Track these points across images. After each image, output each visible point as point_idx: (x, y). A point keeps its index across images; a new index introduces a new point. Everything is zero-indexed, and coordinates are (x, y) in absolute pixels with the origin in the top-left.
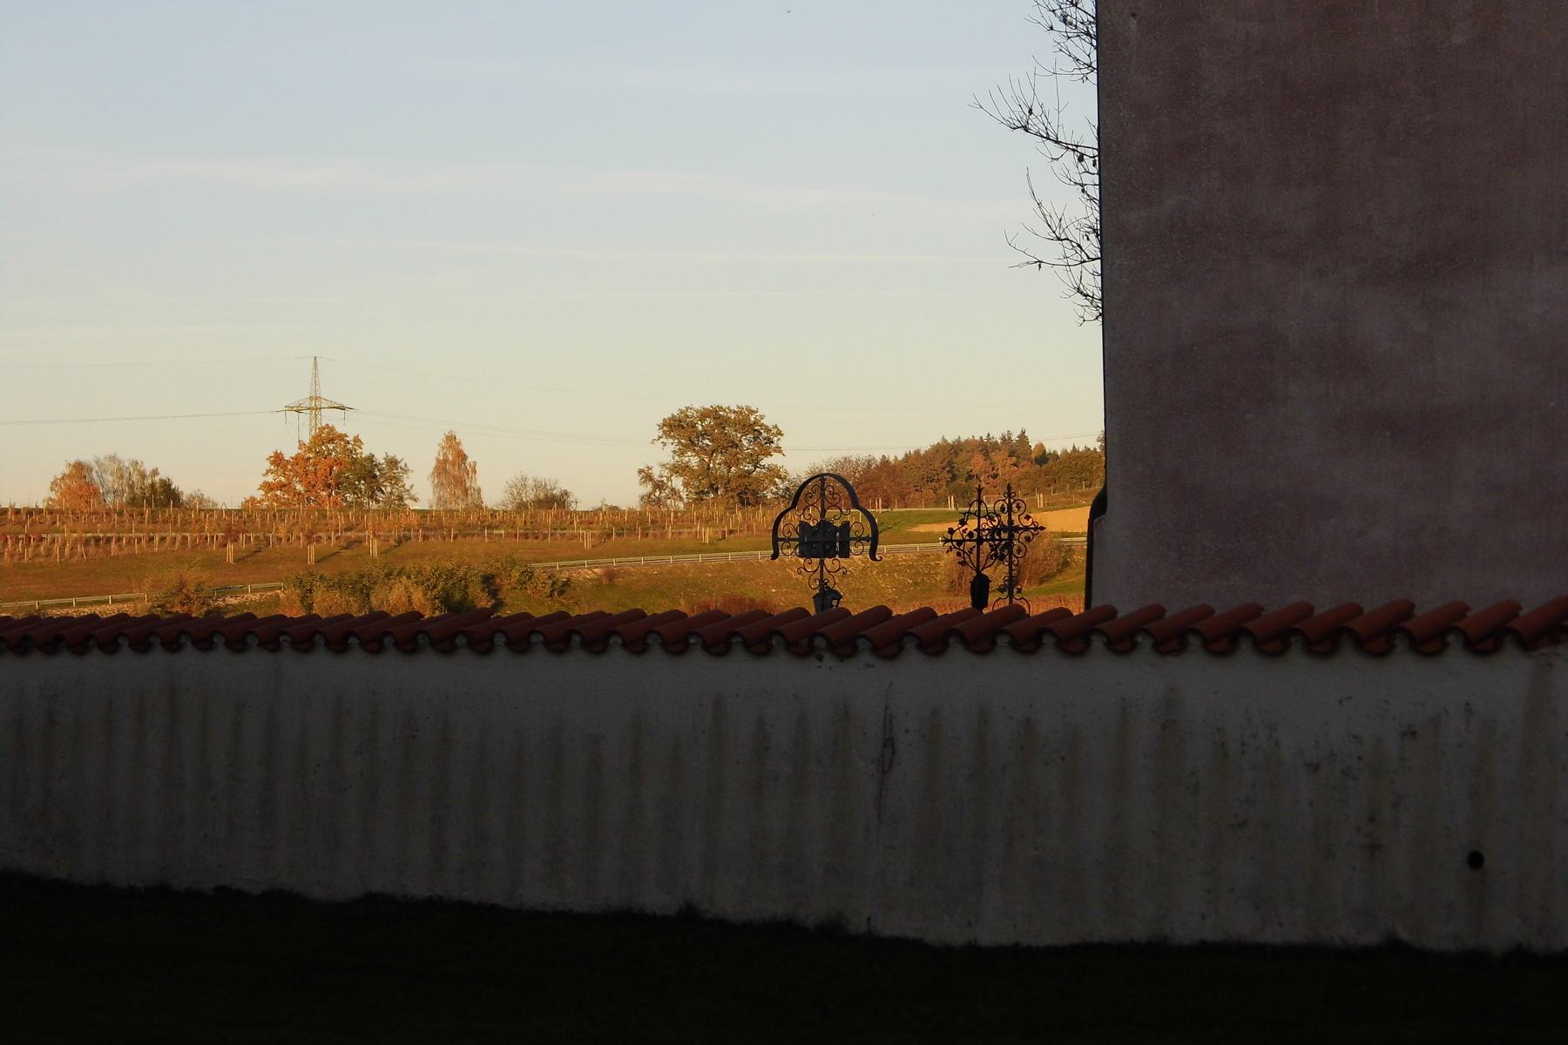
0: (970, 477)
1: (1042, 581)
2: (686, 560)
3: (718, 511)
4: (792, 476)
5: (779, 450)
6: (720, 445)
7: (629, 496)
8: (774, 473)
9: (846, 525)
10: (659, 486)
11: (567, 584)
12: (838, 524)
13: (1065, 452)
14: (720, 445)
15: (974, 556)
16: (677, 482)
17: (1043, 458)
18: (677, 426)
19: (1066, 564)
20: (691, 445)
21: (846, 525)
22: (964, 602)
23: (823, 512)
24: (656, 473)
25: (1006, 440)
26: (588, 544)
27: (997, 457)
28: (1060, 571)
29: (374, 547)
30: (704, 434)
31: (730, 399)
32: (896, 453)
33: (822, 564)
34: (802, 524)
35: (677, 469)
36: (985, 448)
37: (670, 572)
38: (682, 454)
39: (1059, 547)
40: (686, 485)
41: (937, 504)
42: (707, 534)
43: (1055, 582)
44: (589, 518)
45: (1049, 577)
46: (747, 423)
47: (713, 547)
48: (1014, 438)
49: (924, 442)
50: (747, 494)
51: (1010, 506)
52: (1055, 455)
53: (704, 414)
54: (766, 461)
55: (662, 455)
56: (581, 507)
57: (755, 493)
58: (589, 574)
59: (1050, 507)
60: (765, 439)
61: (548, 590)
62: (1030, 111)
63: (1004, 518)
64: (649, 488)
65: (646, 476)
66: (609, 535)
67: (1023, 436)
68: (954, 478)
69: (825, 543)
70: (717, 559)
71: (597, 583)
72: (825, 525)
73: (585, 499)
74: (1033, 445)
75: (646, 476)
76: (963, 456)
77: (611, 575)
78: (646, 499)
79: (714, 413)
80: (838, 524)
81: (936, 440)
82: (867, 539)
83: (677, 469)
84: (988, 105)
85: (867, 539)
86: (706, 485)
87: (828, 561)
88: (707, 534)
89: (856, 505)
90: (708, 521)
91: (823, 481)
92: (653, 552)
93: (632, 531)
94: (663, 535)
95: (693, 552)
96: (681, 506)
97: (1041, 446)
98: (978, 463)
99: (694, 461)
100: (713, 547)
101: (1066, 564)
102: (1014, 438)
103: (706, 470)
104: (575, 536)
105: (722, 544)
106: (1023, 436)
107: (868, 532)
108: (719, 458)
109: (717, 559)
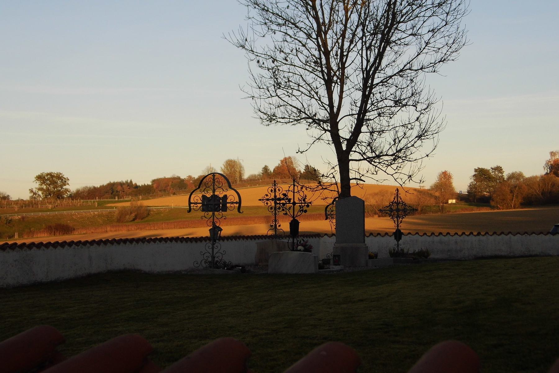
0: (117, 192)
1: (142, 219)
2: (44, 214)
3: (53, 200)
4: (72, 191)
5: (68, 184)
6: (52, 183)
7: (26, 196)
8: (67, 190)
9: (225, 197)
10: (35, 194)
11: (11, 220)
12: (221, 196)
14: (52, 183)
15: (291, 211)
16: (40, 193)
17: (136, 187)
18: (40, 178)
19: (148, 214)
20: (44, 183)
21: (225, 197)
22: (334, 237)
24: (34, 190)
25: (127, 182)
26: (16, 210)
27: (124, 186)
30: (48, 180)
31: (55, 170)
32: (98, 185)
33: (214, 214)
35: (40, 189)
36: (121, 184)
37: (40, 217)
38: (41, 185)
39: (147, 210)
40: (42, 193)
41: (112, 198)
42: (50, 206)
43: (146, 219)
44: (17, 202)
46: (59, 177)
47: (52, 210)
48: (129, 181)
49: (105, 183)
50: (59, 195)
51: (275, 190)
52: (139, 186)
53: (48, 174)
54: (64, 187)
55: (36, 185)
56: (13, 199)
57: (61, 196)
58: (17, 218)
59: (143, 199)
60: (64, 181)
61: (5, 222)
62: (246, 40)
63: (273, 194)
64: (32, 194)
65: (31, 191)
66: (22, 207)
67: (131, 181)
68: (113, 192)
69: (215, 205)
70: (52, 213)
71: (19, 220)
72: (214, 197)
73: (14, 197)
74: (134, 183)
75: (31, 191)
76: (115, 186)
77: (23, 218)
78: (32, 197)
79: (50, 174)
80: (221, 196)
81: (108, 182)
82: (236, 203)
83: (40, 189)
84: (228, 37)
85: (236, 203)
86: (47, 193)
87: (216, 213)
88: (50, 206)
90: (50, 203)
92: (35, 211)
93: (29, 206)
94: (38, 207)
95: (46, 211)
96: (41, 199)
97: (136, 184)
98: (119, 188)
99: (45, 187)
100: (52, 210)
101: (148, 214)
102: (129, 181)
103: (48, 189)
104: (13, 207)
105: (54, 209)
106: (131, 181)
107: (237, 200)
108: (52, 186)
109: (52, 213)
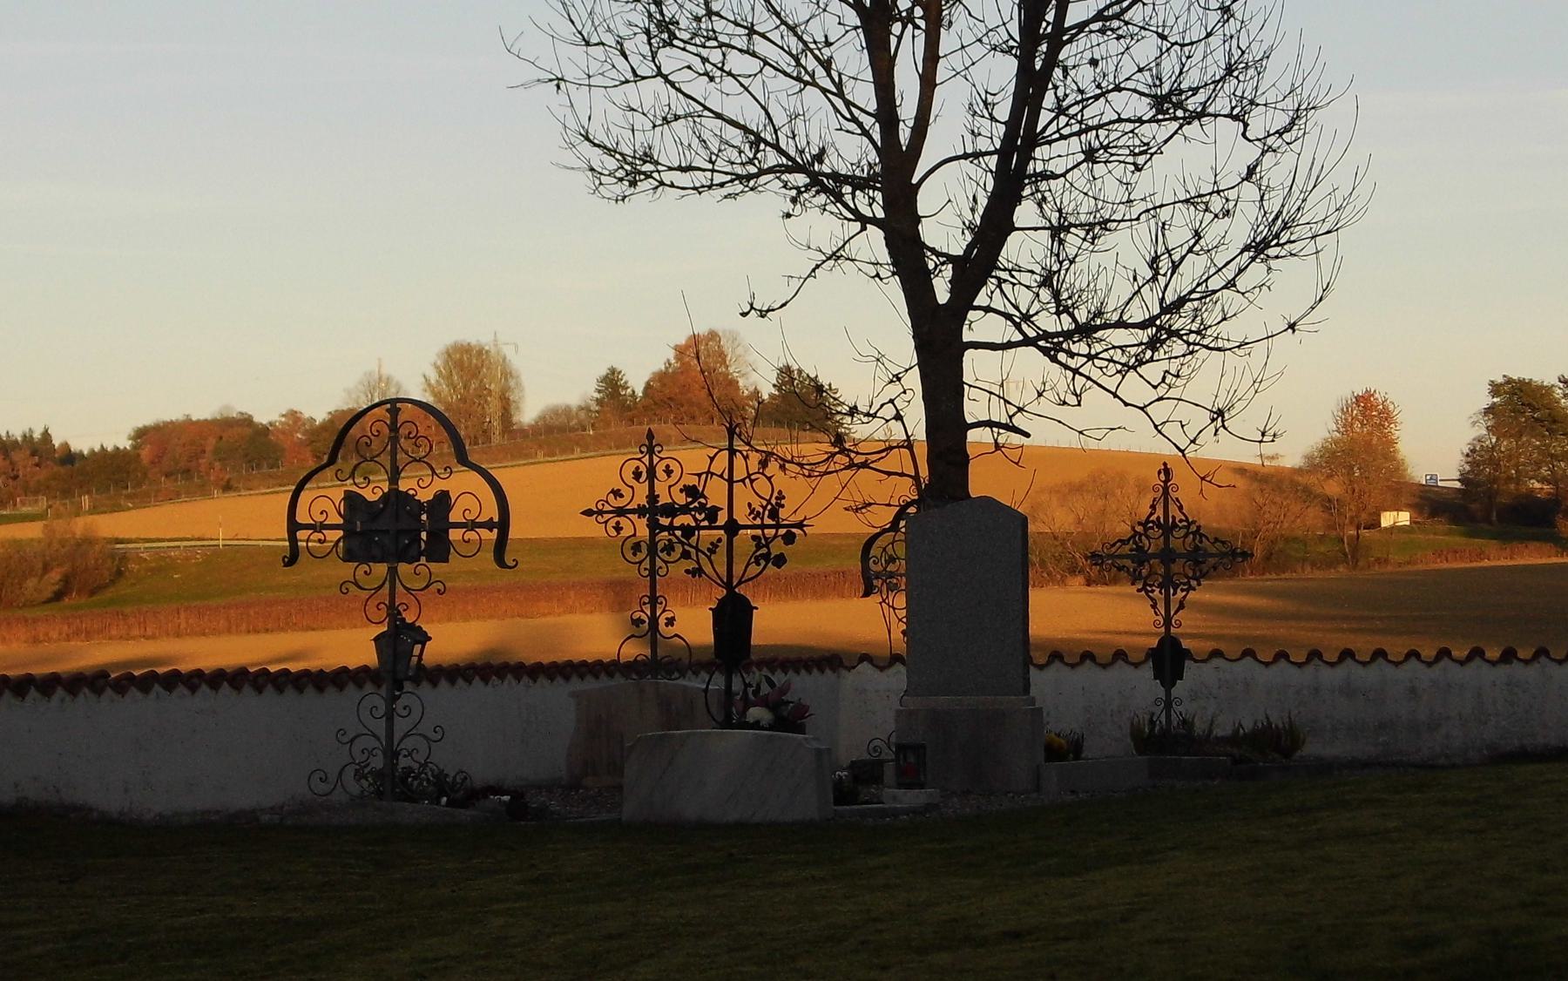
1: (92, 593)
9: (443, 500)
12: (425, 496)
13: (92, 452)
17: (69, 457)
19: (119, 573)
21: (443, 500)
23: (394, 477)
25: (28, 438)
27: (17, 456)
28: (113, 582)
29: (106, 573)
33: (393, 572)
34: (351, 499)
39: (112, 556)
43: (109, 593)
45: (100, 588)
48: (37, 435)
52: (81, 455)
67: (46, 435)
72: (397, 500)
74: (57, 443)
80: (425, 496)
82: (489, 525)
85: (489, 525)
87: (403, 568)
89: (463, 459)
91: (394, 412)
97: (66, 446)
101: (119, 573)
102: (37, 435)
106: (46, 435)
